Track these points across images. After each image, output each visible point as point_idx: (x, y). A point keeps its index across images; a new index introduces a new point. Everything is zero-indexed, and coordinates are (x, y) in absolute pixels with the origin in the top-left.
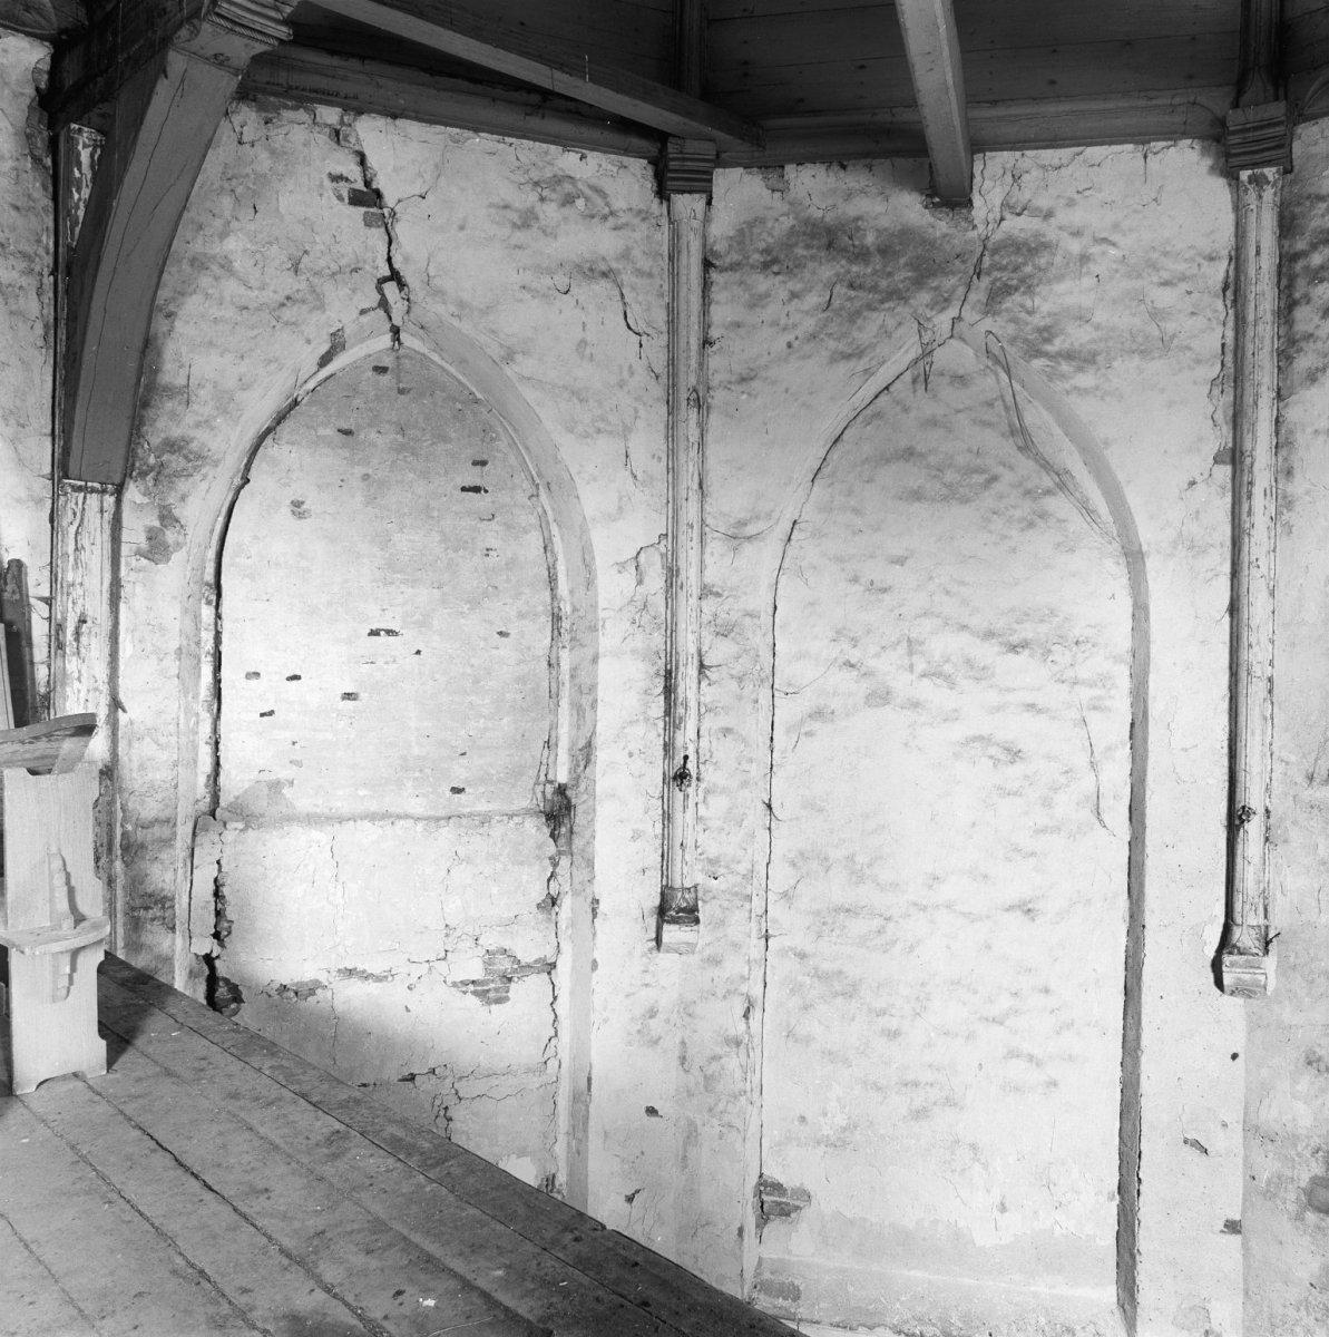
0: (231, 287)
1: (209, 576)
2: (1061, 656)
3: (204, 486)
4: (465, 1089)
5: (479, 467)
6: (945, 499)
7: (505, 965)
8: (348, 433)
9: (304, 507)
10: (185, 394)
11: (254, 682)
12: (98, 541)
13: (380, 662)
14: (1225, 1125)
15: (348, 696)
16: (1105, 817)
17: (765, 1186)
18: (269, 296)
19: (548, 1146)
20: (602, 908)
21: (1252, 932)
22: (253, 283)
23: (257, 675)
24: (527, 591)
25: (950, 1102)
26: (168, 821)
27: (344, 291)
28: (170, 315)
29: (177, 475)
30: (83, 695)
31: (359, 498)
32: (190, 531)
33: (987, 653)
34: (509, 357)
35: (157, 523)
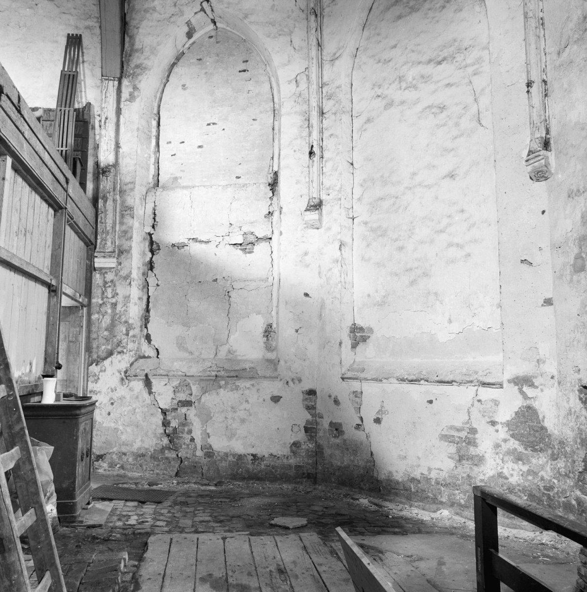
0: (156, 16)
1: (155, 111)
2: (459, 58)
3: (146, 77)
4: (237, 285)
5: (245, 63)
6: (410, 13)
7: (251, 238)
8: (200, 60)
9: (186, 86)
10: (141, 51)
11: (169, 145)
12: (112, 95)
13: (210, 134)
14: (540, 249)
15: (200, 147)
16: (482, 122)
17: (355, 329)
18: (167, 16)
19: (269, 312)
20: (284, 210)
21: (537, 140)
22: (162, 13)
23: (170, 142)
24: (264, 103)
25: (426, 275)
26: (133, 183)
27: (190, 8)
28: (138, 28)
29: (138, 75)
30: (106, 142)
31: (204, 80)
32: (142, 91)
33: (429, 69)
34: (246, 17)
35: (132, 90)
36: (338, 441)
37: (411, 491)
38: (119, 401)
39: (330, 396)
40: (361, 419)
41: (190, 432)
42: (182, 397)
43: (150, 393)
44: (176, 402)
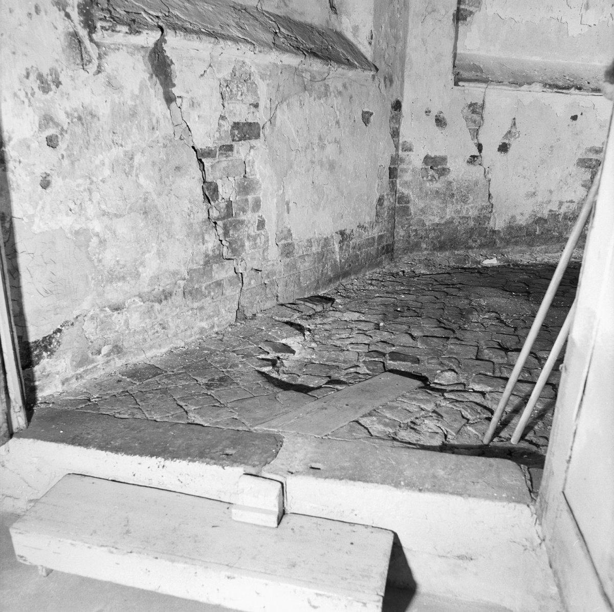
36: (438, 185)
37: (535, 235)
38: (78, 129)
39: (428, 112)
40: (480, 147)
41: (257, 205)
42: (241, 113)
43: (169, 99)
44: (227, 126)
